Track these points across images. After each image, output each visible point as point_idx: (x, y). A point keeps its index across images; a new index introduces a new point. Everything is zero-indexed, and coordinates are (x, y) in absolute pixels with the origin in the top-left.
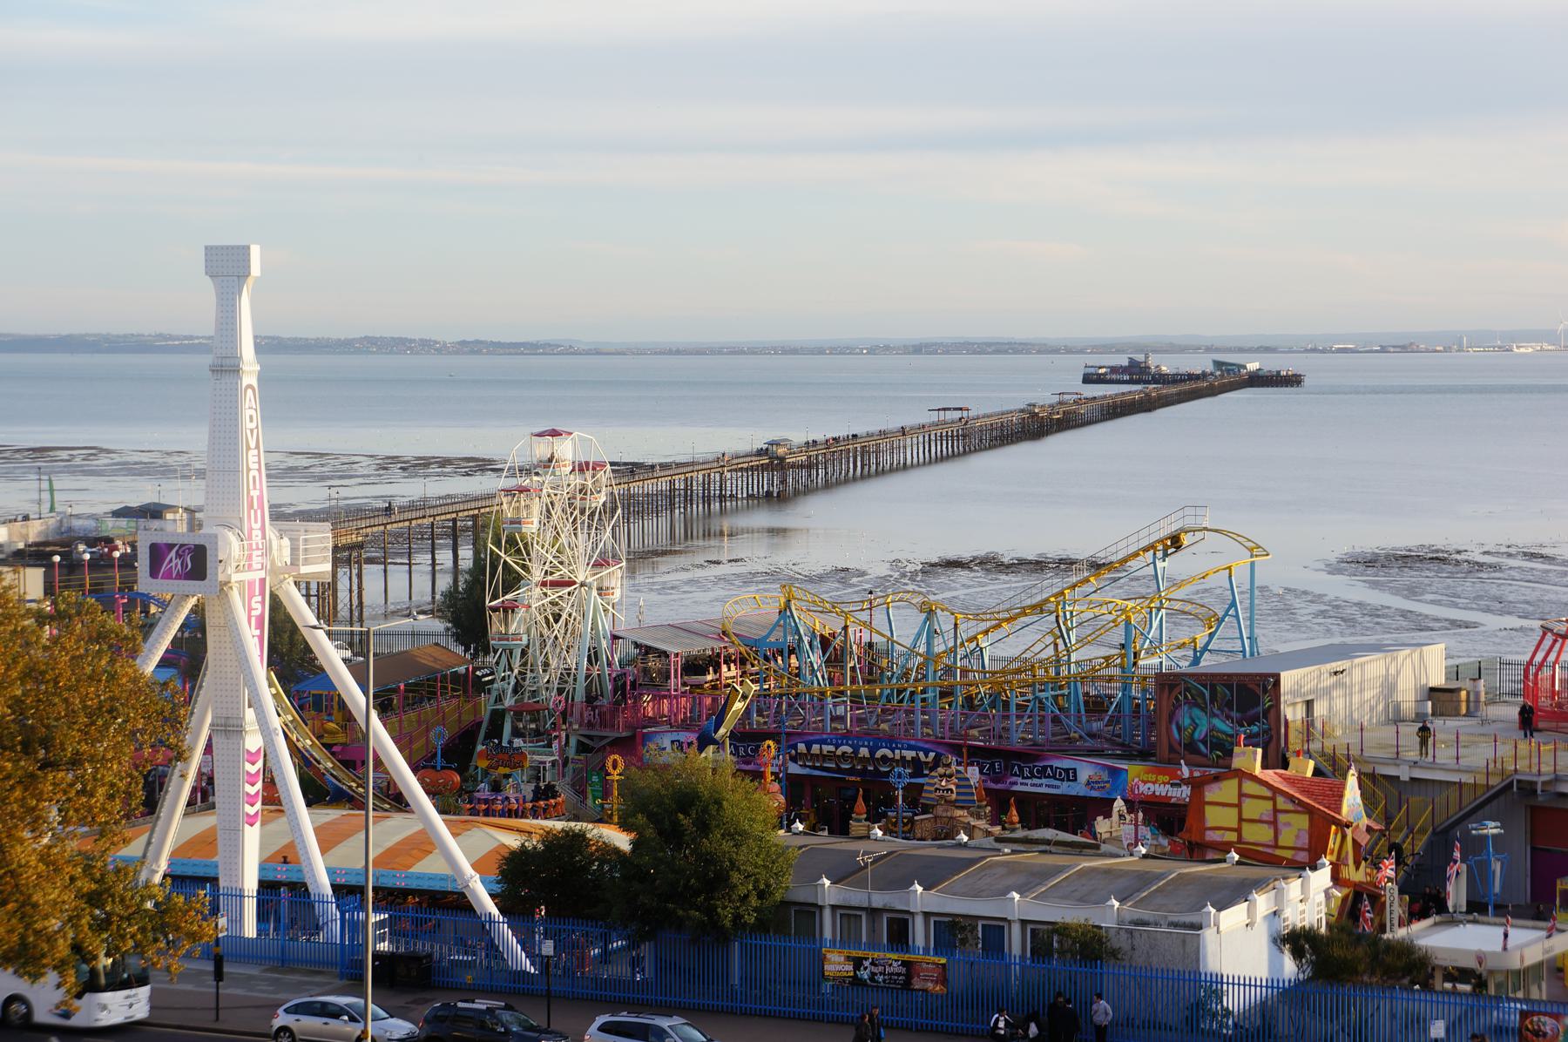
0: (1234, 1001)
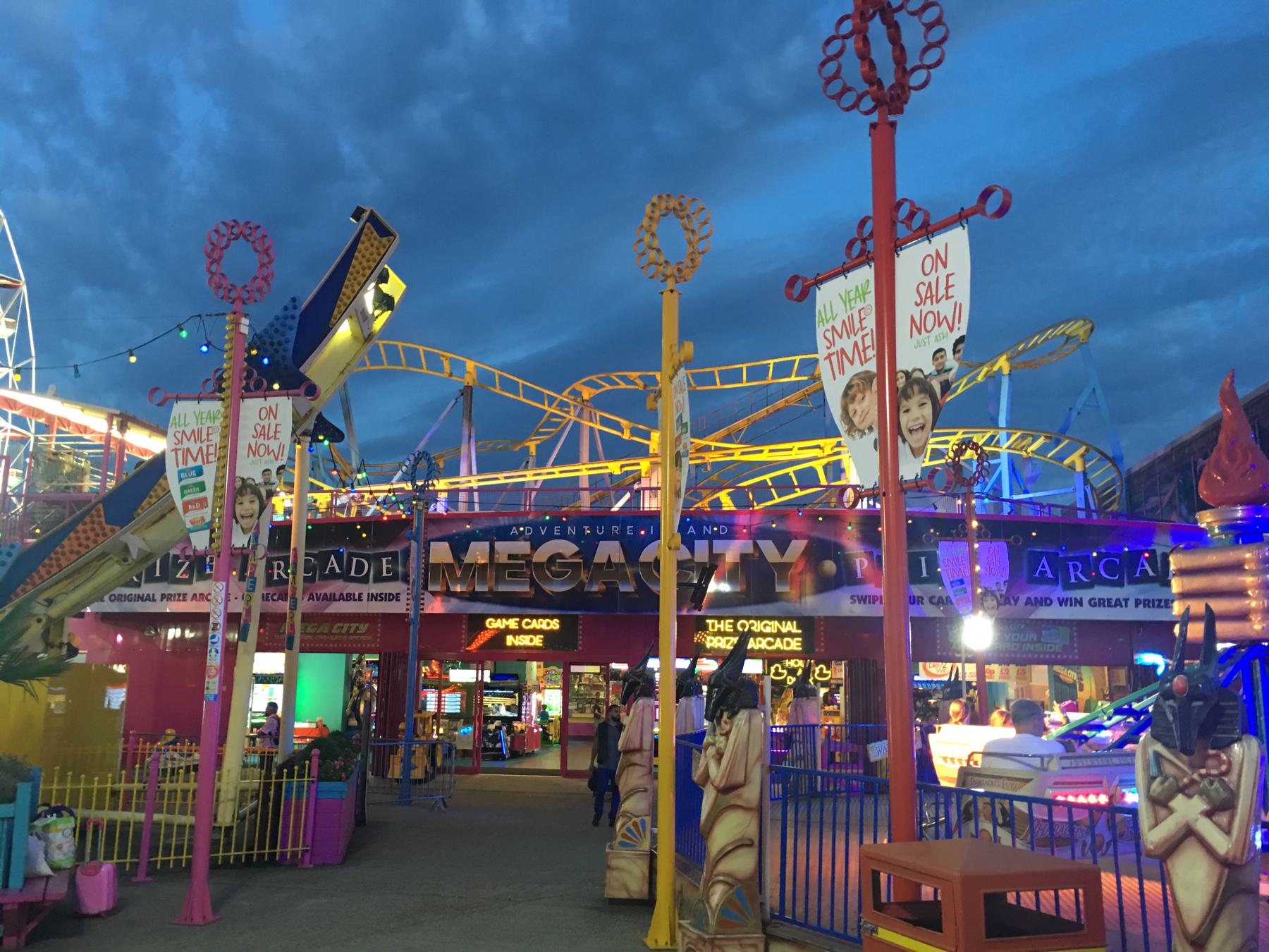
0: (340, 730)
